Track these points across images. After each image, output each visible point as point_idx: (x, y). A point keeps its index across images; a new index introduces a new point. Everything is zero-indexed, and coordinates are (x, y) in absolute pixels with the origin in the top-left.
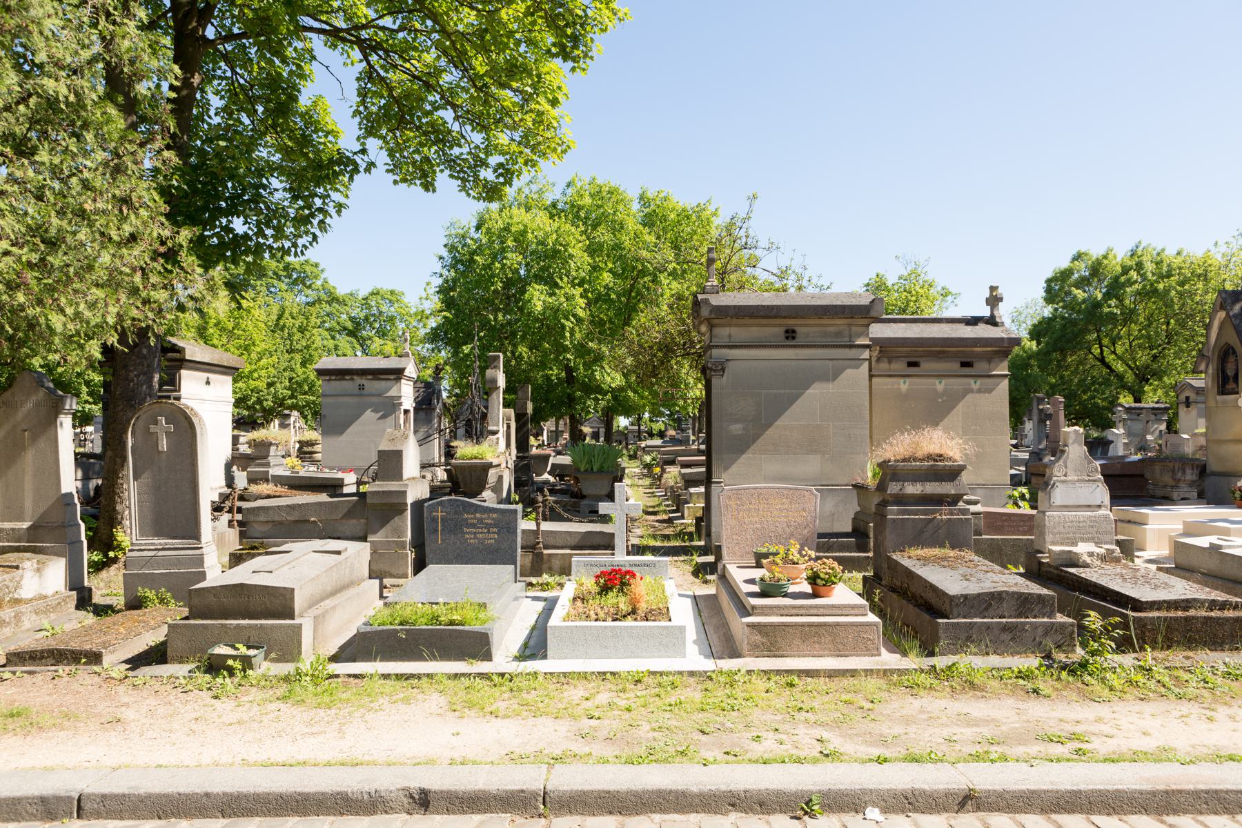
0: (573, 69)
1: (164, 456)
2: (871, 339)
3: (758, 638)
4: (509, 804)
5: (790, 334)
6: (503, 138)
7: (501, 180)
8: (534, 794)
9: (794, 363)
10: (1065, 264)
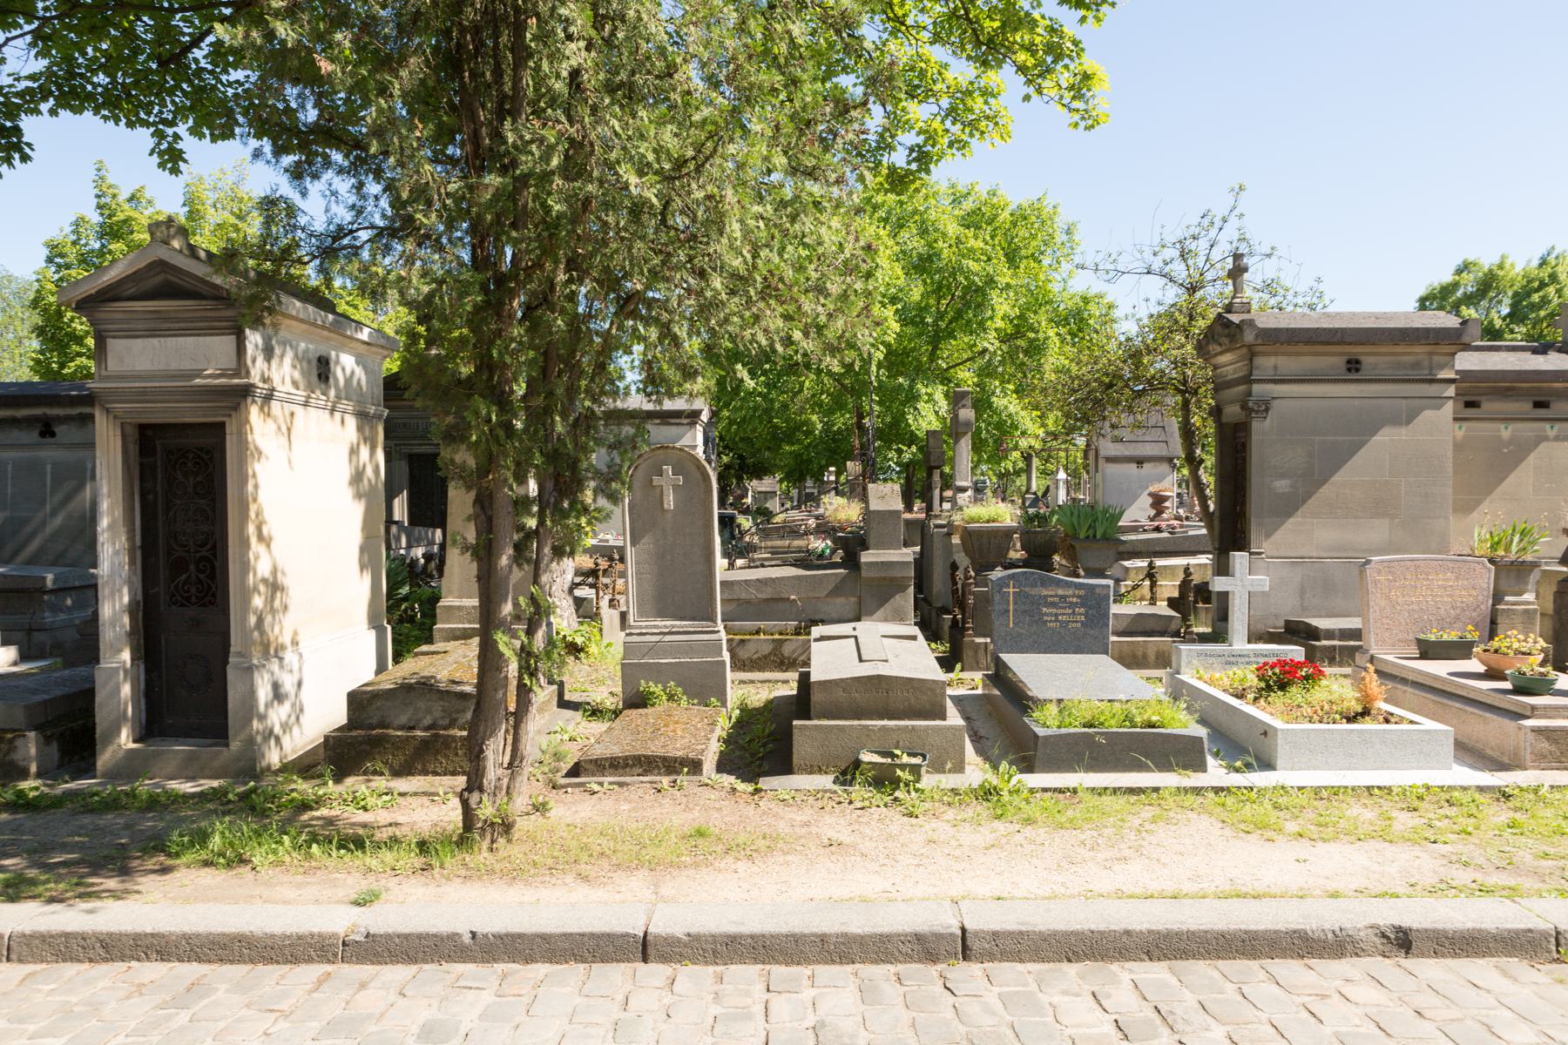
0: (1083, 19)
1: (669, 515)
2: (1458, 372)
3: (1545, 745)
4: (1514, 947)
5: (1353, 365)
6: (919, 112)
7: (914, 166)
8: (1544, 935)
9: (1357, 402)
10: (1447, 277)
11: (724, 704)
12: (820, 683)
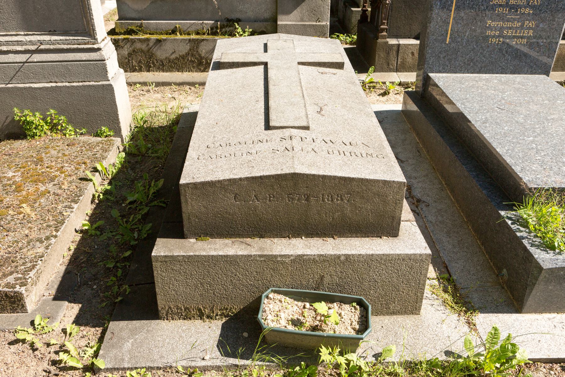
11: (118, 133)
12: (195, 186)
